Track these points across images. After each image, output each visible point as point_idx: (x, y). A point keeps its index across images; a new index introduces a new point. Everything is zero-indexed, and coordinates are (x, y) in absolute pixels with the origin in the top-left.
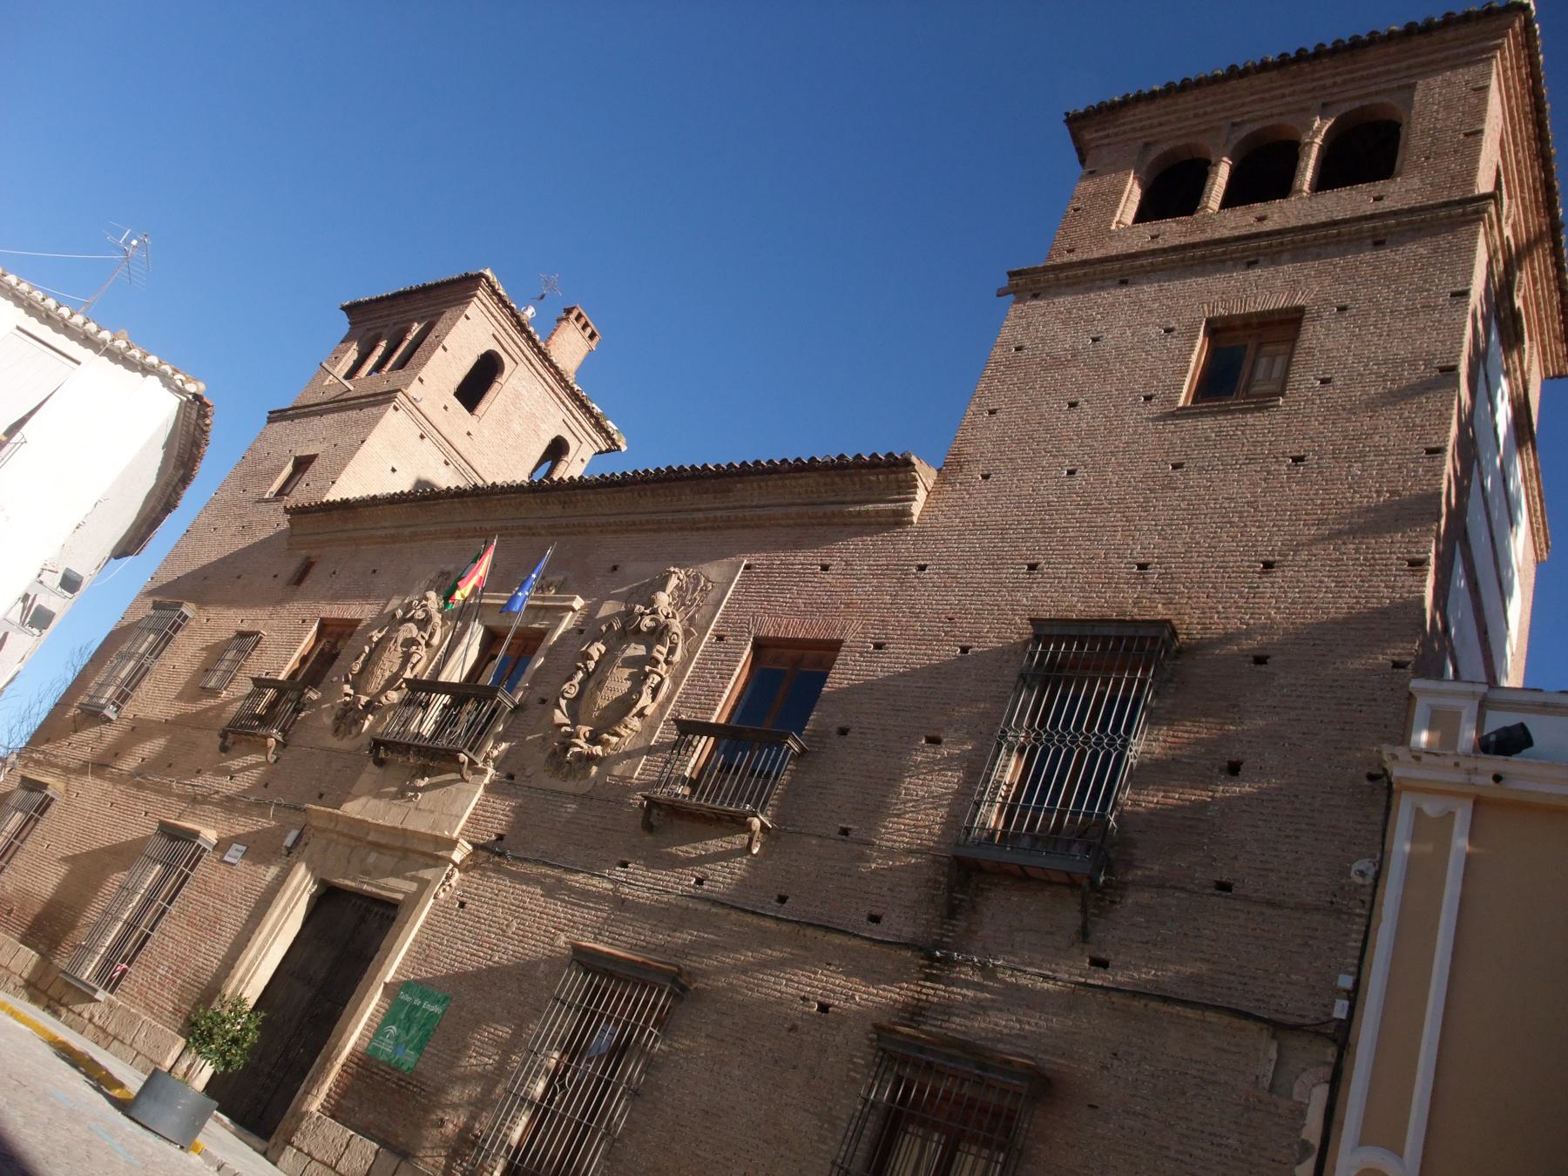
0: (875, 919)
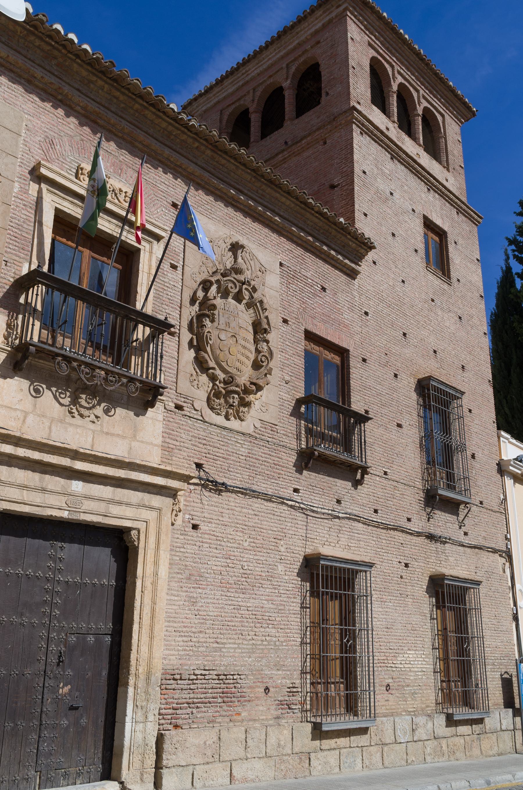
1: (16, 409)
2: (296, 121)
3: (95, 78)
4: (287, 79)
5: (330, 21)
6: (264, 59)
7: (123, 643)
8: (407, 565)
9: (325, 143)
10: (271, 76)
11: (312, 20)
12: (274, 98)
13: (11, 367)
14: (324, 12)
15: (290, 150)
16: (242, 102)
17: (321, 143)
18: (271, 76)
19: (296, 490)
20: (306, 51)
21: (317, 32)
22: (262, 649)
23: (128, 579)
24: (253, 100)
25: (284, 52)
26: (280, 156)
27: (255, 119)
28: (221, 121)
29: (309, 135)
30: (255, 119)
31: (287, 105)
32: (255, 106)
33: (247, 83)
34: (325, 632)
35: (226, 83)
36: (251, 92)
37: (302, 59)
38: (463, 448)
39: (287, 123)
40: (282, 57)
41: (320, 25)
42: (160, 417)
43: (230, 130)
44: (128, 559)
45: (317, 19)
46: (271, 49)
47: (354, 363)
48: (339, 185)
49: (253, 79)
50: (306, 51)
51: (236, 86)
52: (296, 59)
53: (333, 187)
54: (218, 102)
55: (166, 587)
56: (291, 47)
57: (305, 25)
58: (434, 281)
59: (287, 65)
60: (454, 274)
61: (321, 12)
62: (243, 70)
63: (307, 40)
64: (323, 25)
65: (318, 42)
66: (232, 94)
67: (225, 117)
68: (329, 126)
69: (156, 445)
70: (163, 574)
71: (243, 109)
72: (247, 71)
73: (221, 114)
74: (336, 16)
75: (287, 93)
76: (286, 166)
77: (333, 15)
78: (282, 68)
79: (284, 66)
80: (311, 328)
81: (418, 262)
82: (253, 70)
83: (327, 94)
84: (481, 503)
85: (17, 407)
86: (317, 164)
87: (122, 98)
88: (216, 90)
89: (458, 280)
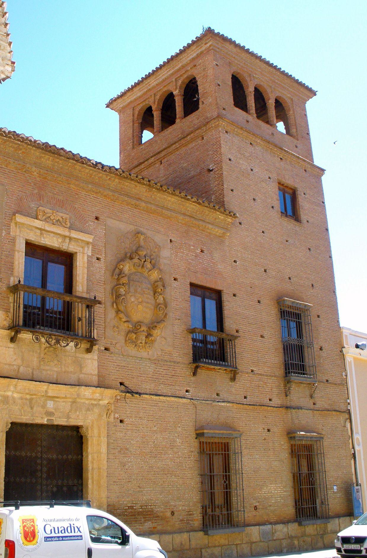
0: (245, 398)
1: (13, 365)
2: (184, 120)
3: (44, 155)
4: (176, 89)
5: (202, 53)
6: (159, 75)
7: (84, 490)
8: (269, 430)
9: (203, 138)
10: (165, 86)
11: (189, 51)
12: (168, 102)
13: (9, 341)
14: (197, 47)
15: (179, 142)
16: (147, 103)
17: (200, 138)
18: (165, 86)
19: (187, 391)
20: (187, 71)
21: (193, 59)
22: (169, 490)
23: (84, 454)
24: (154, 102)
25: (173, 71)
26: (174, 146)
27: (157, 115)
28: (133, 115)
29: (192, 132)
30: (157, 115)
31: (177, 108)
32: (156, 106)
33: (150, 90)
34: (211, 478)
35: (135, 90)
36: (153, 96)
37: (185, 76)
38: (311, 345)
39: (178, 121)
40: (172, 74)
41: (195, 55)
42: (96, 357)
43: (140, 121)
44: (82, 443)
45: (192, 51)
46: (164, 69)
47: (225, 298)
48: (213, 169)
49: (154, 88)
50: (187, 71)
51: (142, 92)
52: (181, 76)
53: (210, 171)
54: (131, 102)
55: (106, 458)
56: (177, 68)
57: (184, 55)
58: (288, 224)
59: (176, 79)
60: (303, 217)
61: (195, 47)
62: (146, 82)
63: (187, 64)
64: (197, 55)
65: (195, 66)
66: (140, 97)
67: (136, 113)
68: (204, 128)
69: (95, 375)
70: (104, 451)
71: (149, 106)
72: (148, 83)
73: (133, 110)
74: (206, 49)
75: (176, 98)
76: (178, 153)
77: (203, 48)
78: (172, 81)
79: (174, 80)
80: (193, 281)
81: (275, 214)
82: (153, 82)
83: (203, 103)
84: (327, 381)
85: (14, 363)
86: (198, 153)
87: (60, 162)
88: (129, 94)
89: (308, 222)
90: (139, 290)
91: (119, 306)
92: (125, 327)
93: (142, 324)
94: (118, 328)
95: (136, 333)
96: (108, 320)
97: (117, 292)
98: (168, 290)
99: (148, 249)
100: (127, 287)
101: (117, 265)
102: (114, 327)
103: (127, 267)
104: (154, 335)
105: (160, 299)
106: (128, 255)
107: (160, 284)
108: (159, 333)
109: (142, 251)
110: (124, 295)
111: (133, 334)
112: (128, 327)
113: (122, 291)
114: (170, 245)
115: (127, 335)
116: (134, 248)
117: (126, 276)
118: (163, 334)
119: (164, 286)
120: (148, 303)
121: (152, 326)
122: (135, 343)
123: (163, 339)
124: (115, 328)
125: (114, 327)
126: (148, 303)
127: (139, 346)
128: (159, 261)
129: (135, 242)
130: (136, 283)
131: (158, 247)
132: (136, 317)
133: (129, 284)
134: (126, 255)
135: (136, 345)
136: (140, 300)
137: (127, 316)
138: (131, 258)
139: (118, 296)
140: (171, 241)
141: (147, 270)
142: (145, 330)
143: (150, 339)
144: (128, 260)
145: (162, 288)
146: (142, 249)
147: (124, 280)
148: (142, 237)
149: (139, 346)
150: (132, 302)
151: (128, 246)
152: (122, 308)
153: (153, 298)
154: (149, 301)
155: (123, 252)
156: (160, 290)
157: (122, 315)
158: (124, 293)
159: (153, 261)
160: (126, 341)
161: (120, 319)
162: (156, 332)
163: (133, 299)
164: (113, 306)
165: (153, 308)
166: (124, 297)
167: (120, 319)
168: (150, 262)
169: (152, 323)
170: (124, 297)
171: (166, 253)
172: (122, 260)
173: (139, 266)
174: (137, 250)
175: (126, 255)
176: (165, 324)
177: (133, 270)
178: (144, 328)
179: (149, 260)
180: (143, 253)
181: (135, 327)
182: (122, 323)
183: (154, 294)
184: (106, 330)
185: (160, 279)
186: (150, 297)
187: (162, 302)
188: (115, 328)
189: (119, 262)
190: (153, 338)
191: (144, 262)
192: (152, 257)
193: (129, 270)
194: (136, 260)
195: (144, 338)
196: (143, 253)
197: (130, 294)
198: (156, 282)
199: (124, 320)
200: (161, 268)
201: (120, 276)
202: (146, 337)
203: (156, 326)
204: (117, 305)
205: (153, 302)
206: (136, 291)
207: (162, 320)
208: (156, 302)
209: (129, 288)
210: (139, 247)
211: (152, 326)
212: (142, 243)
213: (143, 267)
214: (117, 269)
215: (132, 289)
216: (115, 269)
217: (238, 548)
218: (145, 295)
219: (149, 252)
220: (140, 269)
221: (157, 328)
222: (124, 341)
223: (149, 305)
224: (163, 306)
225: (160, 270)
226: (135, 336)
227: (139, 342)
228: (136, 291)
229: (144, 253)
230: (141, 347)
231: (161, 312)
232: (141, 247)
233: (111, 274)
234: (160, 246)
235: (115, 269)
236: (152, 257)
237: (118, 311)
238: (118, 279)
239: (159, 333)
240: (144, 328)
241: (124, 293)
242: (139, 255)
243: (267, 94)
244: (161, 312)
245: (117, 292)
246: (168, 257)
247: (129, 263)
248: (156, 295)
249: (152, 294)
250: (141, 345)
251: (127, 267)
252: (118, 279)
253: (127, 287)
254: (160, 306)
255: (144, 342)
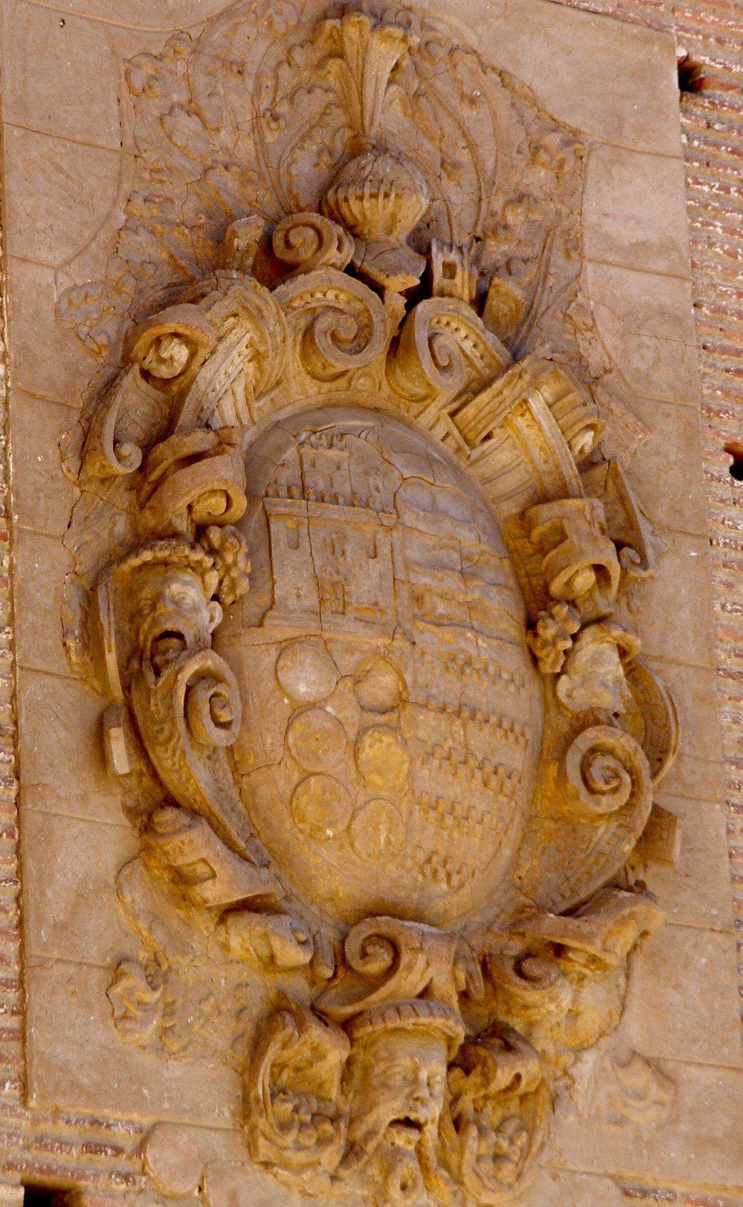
90: (367, 581)
91: (164, 760)
92: (229, 967)
93: (408, 932)
94: (156, 974)
95: (347, 1026)
96: (54, 903)
97: (135, 616)
98: (671, 575)
99: (448, 166)
100: (238, 557)
101: (128, 340)
102: (117, 969)
103: (235, 361)
104: (543, 1041)
105: (596, 674)
106: (246, 235)
107: (582, 514)
108: (591, 1019)
109: (383, 189)
110: (215, 641)
111: (316, 1032)
112: (270, 962)
113: (190, 599)
114: (674, 119)
115: (258, 1045)
116: (306, 169)
117: (223, 445)
118: (635, 1031)
119: (625, 540)
120: (461, 712)
121: (518, 953)
122: (339, 1125)
123: (639, 1078)
124: (134, 981)
125: (117, 969)
126: (461, 712)
127: (391, 1158)
128: (573, 287)
129: (311, 105)
130: (333, 512)
131: (563, 148)
132: (343, 863)
133: (256, 527)
134: (220, 239)
135: (352, 1151)
136: (383, 685)
137: (250, 848)
138: (275, 268)
139: (151, 652)
140: (690, 79)
141: (448, 387)
142: (446, 987)
143: (503, 1077)
144: (244, 288)
145: (608, 556)
146: (385, 167)
147: (208, 489)
148: (383, 54)
149: (391, 1158)
150: (300, 709)
151: (246, 149)
152: (195, 774)
153: (515, 661)
154: (479, 692)
155: (186, 208)
156: (586, 580)
157: (192, 846)
158: (208, 617)
159: (508, 292)
160: (246, 1108)
161: (182, 880)
162: (555, 1008)
163: (305, 680)
164: (102, 757)
165: (517, 758)
166: (211, 661)
167: (182, 880)
168: (480, 303)
169: (520, 918)
170: (211, 661)
171: (637, 206)
172: (185, 290)
173: (360, 343)
174: (334, 180)
175: (220, 239)
176: (657, 917)
177: (303, 391)
178: (431, 967)
179: (463, 284)
180: (395, 211)
181: (341, 960)
182: (204, 923)
183: (531, 625)
184: (38, 1000)
185: (587, 464)
186: (480, 649)
187: (610, 700)
188: (134, 981)
189: (143, 316)
190: (529, 1069)
191: (414, 297)
192: (496, 250)
193: (255, 392)
194: (324, 286)
195: (435, 1068)
196: (395, 211)
197: (278, 629)
198: (544, 498)
199: (217, 892)
200: (595, 357)
201: (166, 453)
202: (462, 1062)
203: (559, 950)
204: (139, 744)
205: (515, 699)
206: (332, 595)
207: (615, 885)
208: (551, 703)
209: (264, 570)
210: (356, 150)
211: (516, 947)
212: (387, 113)
213: (398, 346)
214: (132, 379)
215: (293, 581)
216: (110, 386)
217: (40, 664)
218: (429, 637)
219: (459, 196)
220: (368, 372)
221: (577, 960)
222: (224, 1114)
223: (480, 739)
224: (623, 741)
225: (589, 380)
226: (336, 1053)
227: (388, 1110)
228: (332, 595)
229: (413, 210)
230: (409, 1167)
231: (610, 803)
232: (380, 149)
233: (71, 439)
234: (573, 138)
235: (110, 386)
236: (496, 250)
237: (156, 804)
238: (146, 484)
239: (591, 1019)
240: (431, 967)
241: (208, 617)
242: (353, 230)
243: (243, 1052)
244: (610, 803)
245: (135, 616)
246: (668, 247)
247: (257, 317)
248: (548, 630)
249: (512, 627)
250: (405, 1139)
251: (235, 361)
252: (146, 484)
253: (238, 557)
254: (592, 736)
255: (430, 1112)
